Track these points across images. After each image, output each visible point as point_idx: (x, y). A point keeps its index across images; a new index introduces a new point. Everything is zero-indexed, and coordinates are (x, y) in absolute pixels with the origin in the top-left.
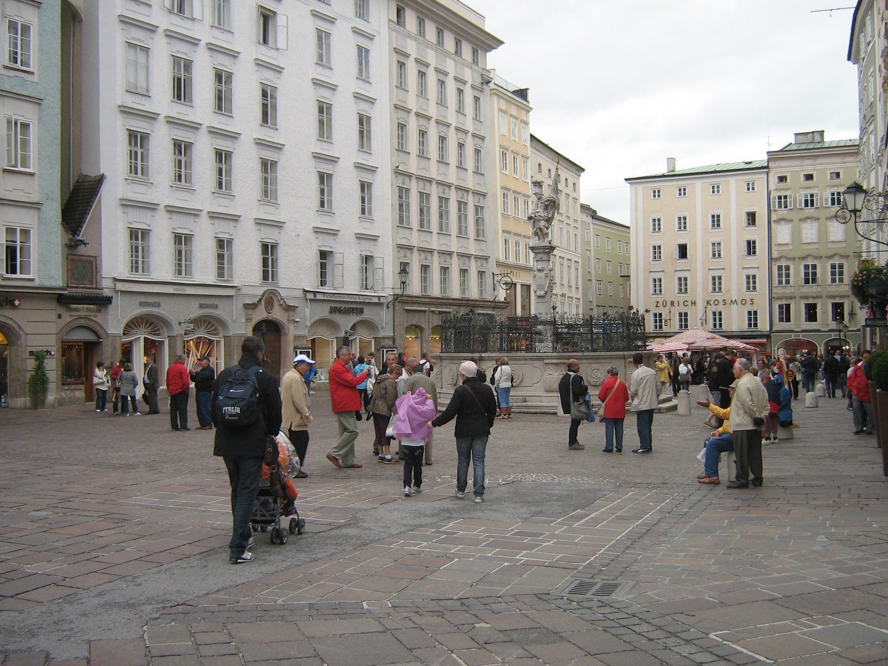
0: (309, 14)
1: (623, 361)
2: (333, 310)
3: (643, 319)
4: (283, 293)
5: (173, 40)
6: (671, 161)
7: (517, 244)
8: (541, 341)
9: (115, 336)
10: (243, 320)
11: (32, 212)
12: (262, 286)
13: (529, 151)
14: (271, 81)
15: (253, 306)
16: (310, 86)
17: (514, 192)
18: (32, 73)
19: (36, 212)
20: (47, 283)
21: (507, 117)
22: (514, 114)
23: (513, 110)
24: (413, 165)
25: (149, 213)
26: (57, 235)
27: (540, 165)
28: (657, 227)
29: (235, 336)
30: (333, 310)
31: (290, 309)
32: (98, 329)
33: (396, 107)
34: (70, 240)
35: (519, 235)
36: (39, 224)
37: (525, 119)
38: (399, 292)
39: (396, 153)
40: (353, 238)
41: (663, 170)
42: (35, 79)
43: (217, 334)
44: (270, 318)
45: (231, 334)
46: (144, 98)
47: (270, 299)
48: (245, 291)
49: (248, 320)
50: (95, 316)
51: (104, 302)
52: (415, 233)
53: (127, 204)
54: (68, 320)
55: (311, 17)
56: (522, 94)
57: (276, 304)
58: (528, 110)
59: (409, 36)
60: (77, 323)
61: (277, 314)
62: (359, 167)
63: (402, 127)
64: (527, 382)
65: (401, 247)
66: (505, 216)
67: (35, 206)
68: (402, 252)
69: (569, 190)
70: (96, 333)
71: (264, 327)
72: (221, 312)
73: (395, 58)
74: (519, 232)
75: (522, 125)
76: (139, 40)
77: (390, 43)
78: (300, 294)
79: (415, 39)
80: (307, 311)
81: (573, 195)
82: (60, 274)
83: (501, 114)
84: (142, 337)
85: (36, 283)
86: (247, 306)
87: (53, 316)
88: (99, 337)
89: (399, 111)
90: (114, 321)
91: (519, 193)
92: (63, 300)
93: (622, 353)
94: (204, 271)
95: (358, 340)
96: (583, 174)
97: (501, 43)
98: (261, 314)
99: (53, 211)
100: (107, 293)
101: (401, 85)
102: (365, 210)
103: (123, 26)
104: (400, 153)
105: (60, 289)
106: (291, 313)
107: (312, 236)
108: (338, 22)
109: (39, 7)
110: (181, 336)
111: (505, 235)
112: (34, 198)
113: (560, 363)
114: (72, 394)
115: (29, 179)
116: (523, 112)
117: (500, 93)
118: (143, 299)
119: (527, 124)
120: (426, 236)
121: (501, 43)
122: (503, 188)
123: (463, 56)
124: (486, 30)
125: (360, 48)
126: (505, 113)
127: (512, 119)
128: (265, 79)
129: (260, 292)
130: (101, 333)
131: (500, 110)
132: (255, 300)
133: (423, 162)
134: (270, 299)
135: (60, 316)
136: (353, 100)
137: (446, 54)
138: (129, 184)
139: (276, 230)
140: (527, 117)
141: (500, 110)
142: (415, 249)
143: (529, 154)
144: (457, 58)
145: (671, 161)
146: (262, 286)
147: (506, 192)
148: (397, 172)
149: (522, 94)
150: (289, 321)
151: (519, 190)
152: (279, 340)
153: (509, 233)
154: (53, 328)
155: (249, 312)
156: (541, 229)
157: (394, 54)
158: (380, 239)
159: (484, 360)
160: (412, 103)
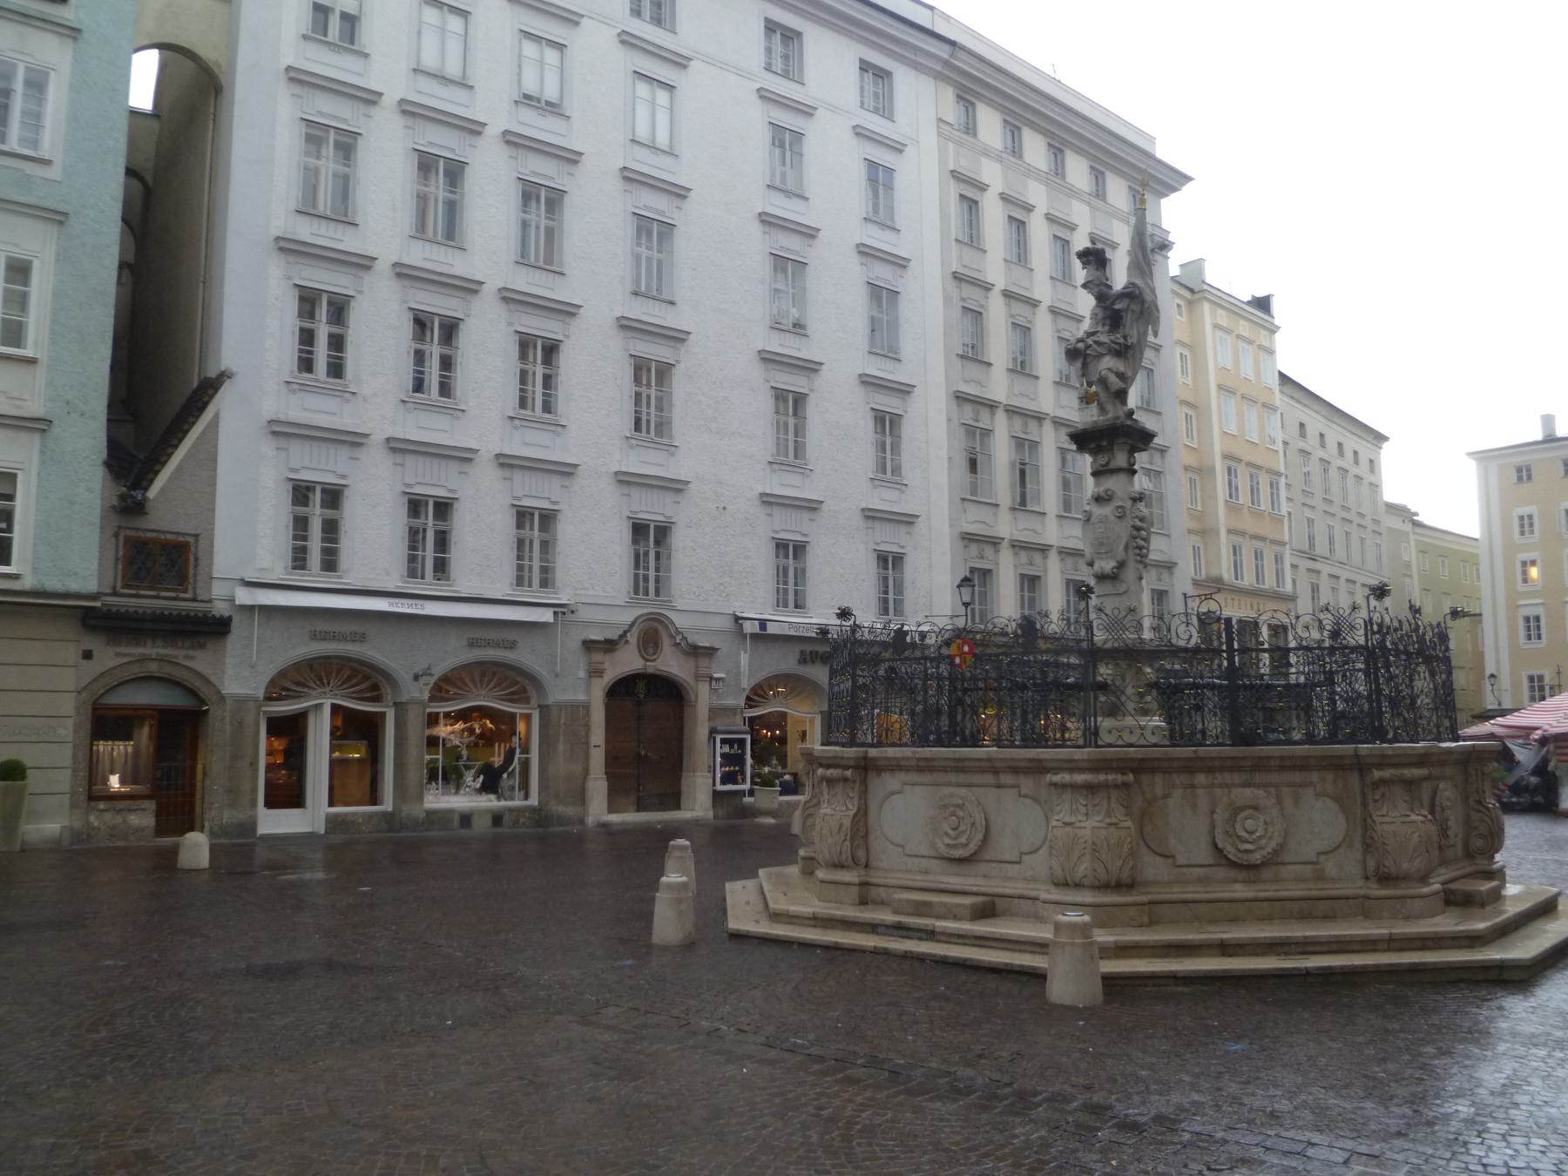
0: (755, 97)
1: (1354, 780)
2: (804, 659)
3: (1443, 637)
4: (679, 621)
5: (419, 121)
6: (1548, 421)
7: (1258, 555)
8: (1113, 711)
9: (241, 701)
10: (582, 674)
11: (23, 437)
12: (629, 605)
13: (1278, 399)
14: (662, 213)
15: (610, 646)
16: (756, 228)
17: (1249, 464)
18: (48, 162)
19: (37, 437)
20: (53, 584)
21: (1229, 339)
22: (1246, 334)
23: (1244, 328)
24: (998, 386)
25: (344, 452)
26: (90, 485)
27: (1322, 435)
28: (1527, 528)
29: (562, 706)
30: (804, 659)
31: (695, 652)
32: (197, 684)
33: (957, 277)
34: (122, 497)
35: (1263, 539)
36: (42, 463)
37: (1266, 344)
38: (961, 623)
39: (958, 363)
40: (858, 520)
41: (1539, 437)
42: (54, 173)
43: (527, 700)
44: (650, 671)
45: (550, 701)
46: (340, 227)
47: (652, 633)
48: (585, 614)
49: (595, 672)
50: (187, 657)
51: (212, 628)
52: (1005, 515)
53: (283, 432)
54: (112, 664)
55: (758, 102)
56: (1263, 304)
57: (666, 642)
58: (1273, 330)
59: (986, 152)
60: (136, 670)
61: (670, 663)
62: (869, 383)
63: (975, 315)
64: (1004, 846)
65: (968, 538)
66: (1233, 507)
67: (38, 425)
68: (974, 548)
69: (1362, 470)
70: (192, 692)
71: (641, 689)
72: (525, 655)
73: (954, 190)
74: (1261, 532)
75: (1262, 354)
76: (335, 117)
77: (942, 162)
78: (726, 624)
79: (999, 159)
80: (744, 659)
81: (1372, 479)
82: (94, 566)
83: (1219, 334)
84: (327, 704)
85: (27, 583)
86: (589, 645)
87: (71, 653)
88: (203, 702)
89: (964, 285)
90: (240, 674)
91: (1259, 468)
92: (97, 620)
93: (1348, 748)
94: (482, 566)
95: (327, 711)
96: (1386, 445)
97: (1188, 179)
98: (628, 661)
99: (86, 436)
100: (220, 609)
101: (972, 239)
102: (888, 466)
103: (296, 89)
104: (968, 364)
105: (896, 766)
106: (704, 662)
107: (759, 512)
108: (820, 113)
109: (75, 39)
110: (420, 703)
111: (1233, 537)
112: (35, 408)
113: (1106, 786)
114: (119, 819)
115: (21, 371)
116: (1263, 332)
117: (1222, 301)
118: (322, 626)
119: (1271, 352)
120: (1032, 522)
121: (1188, 179)
122: (1226, 457)
123: (1110, 200)
124: (1159, 154)
125: (872, 165)
126: (1227, 331)
127: (1241, 344)
128: (646, 207)
129: (627, 617)
130: (205, 691)
131: (1216, 326)
132: (613, 635)
133: (1021, 384)
134: (652, 633)
135: (88, 655)
136: (855, 259)
137: (1073, 192)
138: (293, 391)
139: (669, 498)
140: (1272, 341)
141: (1216, 326)
142: (1005, 544)
143: (1278, 403)
144: (1097, 202)
145: (1548, 421)
146: (629, 605)
147: (1233, 464)
148: (961, 398)
149: (1263, 304)
150: (698, 677)
151: (1259, 462)
152: (681, 707)
153: (1242, 534)
154: (69, 679)
155: (598, 657)
156: (1103, 382)
157: (952, 181)
158: (921, 523)
159: (879, 770)
160: (995, 271)
